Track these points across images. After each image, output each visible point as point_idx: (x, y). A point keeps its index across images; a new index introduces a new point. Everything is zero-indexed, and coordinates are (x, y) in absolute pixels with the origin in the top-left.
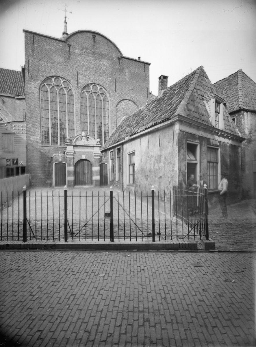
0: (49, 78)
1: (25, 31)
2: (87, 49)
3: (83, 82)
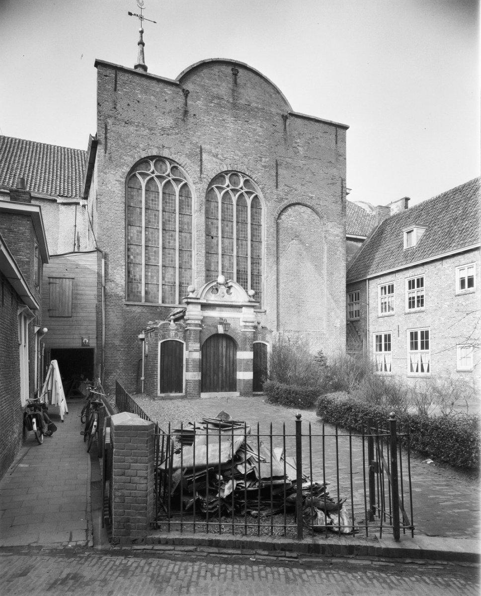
0: (144, 161)
1: (98, 64)
2: (219, 98)
3: (212, 167)
